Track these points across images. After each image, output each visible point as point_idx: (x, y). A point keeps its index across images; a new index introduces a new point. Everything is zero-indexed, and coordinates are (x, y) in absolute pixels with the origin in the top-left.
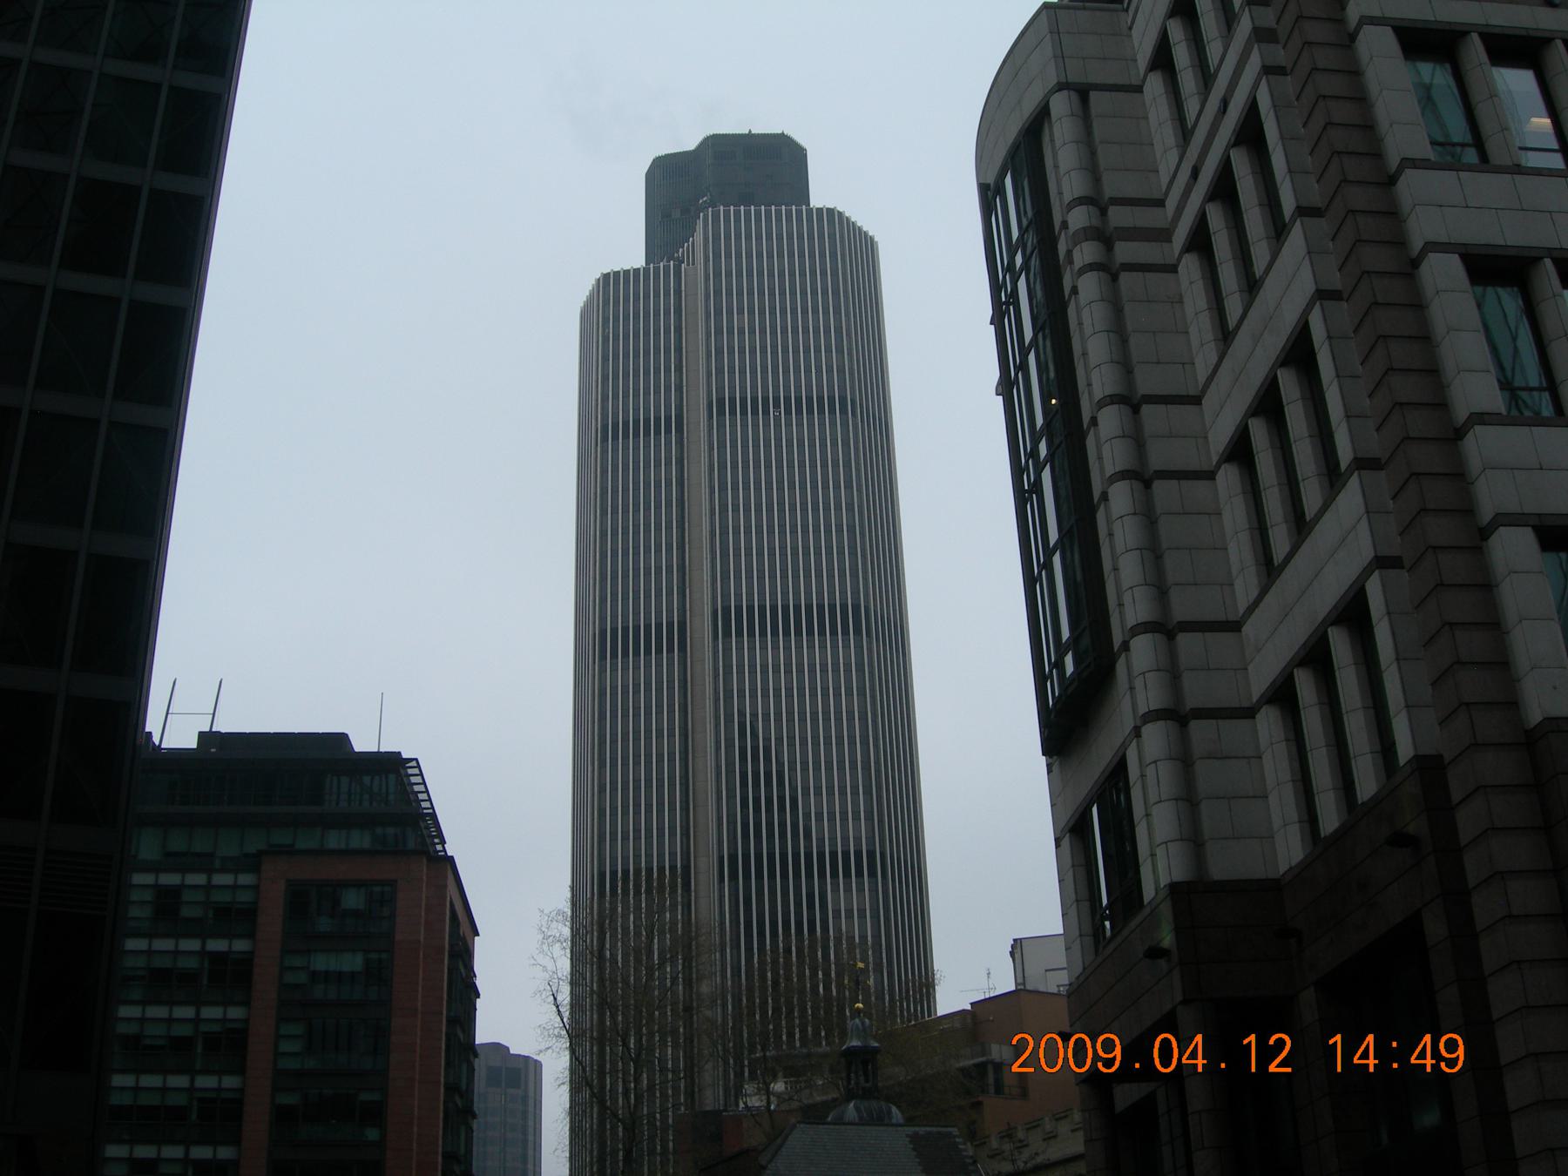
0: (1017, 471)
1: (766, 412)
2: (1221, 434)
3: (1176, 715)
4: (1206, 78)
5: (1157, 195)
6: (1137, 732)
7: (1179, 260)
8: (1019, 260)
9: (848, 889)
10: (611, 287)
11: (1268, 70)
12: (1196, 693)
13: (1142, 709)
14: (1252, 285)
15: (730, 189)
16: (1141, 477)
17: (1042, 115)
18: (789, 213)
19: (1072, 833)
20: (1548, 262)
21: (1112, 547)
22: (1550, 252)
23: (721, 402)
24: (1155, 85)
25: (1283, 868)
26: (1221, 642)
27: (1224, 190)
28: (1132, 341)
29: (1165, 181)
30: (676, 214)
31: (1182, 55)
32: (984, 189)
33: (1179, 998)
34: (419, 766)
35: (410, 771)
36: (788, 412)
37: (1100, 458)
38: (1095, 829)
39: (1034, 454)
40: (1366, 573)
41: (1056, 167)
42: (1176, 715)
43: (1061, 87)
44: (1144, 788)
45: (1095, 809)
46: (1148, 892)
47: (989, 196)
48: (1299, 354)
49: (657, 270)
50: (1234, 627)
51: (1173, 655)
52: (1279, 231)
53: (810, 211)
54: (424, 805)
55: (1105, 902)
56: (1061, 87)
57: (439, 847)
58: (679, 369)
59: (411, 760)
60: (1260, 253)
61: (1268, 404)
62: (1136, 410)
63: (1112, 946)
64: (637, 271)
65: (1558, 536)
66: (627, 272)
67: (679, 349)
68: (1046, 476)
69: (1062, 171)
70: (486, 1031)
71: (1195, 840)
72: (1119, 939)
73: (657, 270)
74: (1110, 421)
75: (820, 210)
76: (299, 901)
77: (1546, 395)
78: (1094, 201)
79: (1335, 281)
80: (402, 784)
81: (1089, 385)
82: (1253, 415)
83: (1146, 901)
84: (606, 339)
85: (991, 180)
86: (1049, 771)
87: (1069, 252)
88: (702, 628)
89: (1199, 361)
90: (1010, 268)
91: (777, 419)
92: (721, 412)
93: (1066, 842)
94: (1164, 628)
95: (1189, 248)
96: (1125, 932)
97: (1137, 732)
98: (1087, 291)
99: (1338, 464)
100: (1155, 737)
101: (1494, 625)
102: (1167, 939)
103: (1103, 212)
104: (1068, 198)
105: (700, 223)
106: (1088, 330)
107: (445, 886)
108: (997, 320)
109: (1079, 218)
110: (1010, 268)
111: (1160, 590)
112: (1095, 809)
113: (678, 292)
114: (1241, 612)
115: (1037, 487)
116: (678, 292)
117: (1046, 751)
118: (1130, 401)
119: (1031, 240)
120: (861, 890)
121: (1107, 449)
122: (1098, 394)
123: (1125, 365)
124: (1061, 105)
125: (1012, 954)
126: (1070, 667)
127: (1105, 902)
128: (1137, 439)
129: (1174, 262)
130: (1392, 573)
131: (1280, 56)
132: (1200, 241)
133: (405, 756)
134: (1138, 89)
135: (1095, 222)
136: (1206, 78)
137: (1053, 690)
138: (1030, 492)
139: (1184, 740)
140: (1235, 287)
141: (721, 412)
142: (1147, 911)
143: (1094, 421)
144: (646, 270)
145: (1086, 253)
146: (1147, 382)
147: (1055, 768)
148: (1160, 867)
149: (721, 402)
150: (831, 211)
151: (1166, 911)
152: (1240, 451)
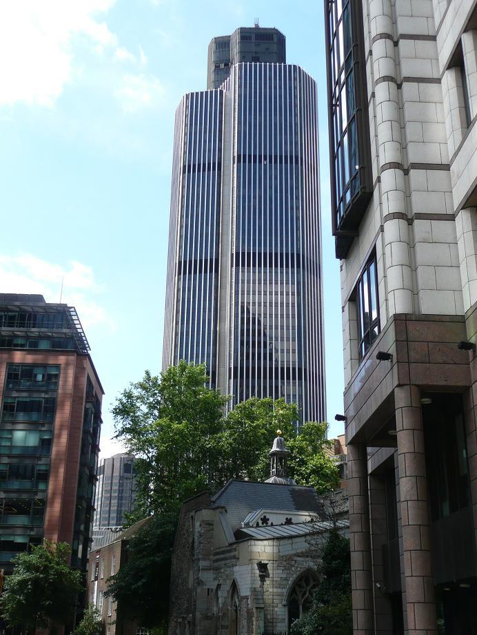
1: (260, 162)
3: (407, 218)
5: (431, 33)
8: (343, 77)
10: (194, 100)
12: (420, 204)
13: (385, 213)
16: (396, 81)
21: (384, 264)
25: (467, 307)
30: (222, 66)
33: (396, 383)
36: (270, 162)
44: (387, 306)
50: (446, 167)
51: (407, 184)
59: (72, 308)
62: (406, 172)
66: (202, 93)
71: (413, 292)
72: (368, 355)
75: (290, 66)
84: (178, 290)
89: (450, 142)
91: (265, 165)
94: (402, 167)
96: (371, 351)
98: (380, 94)
100: (393, 229)
102: (392, 350)
106: (379, 119)
110: (338, 83)
111: (403, 146)
117: (338, 256)
118: (393, 38)
121: (377, 65)
134: (438, 81)
139: (411, 233)
146: (404, 27)
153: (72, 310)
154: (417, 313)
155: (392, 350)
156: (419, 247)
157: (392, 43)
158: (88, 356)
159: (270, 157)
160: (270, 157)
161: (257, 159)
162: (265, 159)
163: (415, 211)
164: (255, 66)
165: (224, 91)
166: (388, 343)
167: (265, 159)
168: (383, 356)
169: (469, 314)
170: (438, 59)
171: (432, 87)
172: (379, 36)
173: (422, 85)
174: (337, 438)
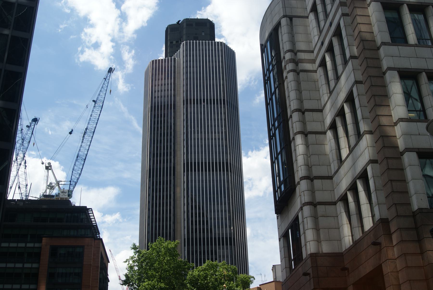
0: (269, 130)
2: (328, 121)
3: (313, 204)
4: (326, 16)
6: (301, 209)
7: (317, 69)
9: (223, 249)
11: (343, 15)
12: (320, 197)
13: (303, 202)
14: (338, 78)
15: (192, 34)
17: (278, 25)
18: (209, 43)
19: (284, 237)
20: (424, 73)
22: (424, 70)
23: (187, 100)
24: (312, 16)
26: (327, 182)
27: (330, 49)
28: (303, 93)
29: (314, 45)
30: (174, 42)
31: (320, 8)
32: (261, 45)
34: (92, 211)
35: (89, 212)
37: (292, 127)
38: (291, 236)
39: (274, 125)
40: (367, 164)
41: (282, 40)
42: (313, 204)
43: (284, 16)
45: (290, 230)
46: (304, 256)
47: (263, 48)
48: (350, 99)
49: (168, 59)
51: (313, 186)
52: (345, 63)
53: (215, 43)
54: (93, 222)
55: (292, 258)
56: (284, 16)
57: (98, 235)
58: (174, 90)
59: (90, 209)
60: (340, 68)
61: (341, 113)
63: (294, 272)
64: (162, 60)
65: (425, 155)
67: (174, 84)
68: (277, 132)
69: (284, 41)
70: (422, 15)
72: (296, 269)
73: (168, 59)
74: (296, 117)
75: (218, 43)
76: (54, 251)
77: (422, 113)
78: (294, 51)
79: (360, 78)
80: (87, 216)
81: (290, 106)
82: (337, 116)
83: (304, 258)
85: (263, 43)
86: (277, 219)
87: (285, 66)
88: (180, 168)
90: (268, 69)
91: (204, 106)
92: (187, 103)
93: (282, 240)
95: (320, 66)
96: (298, 267)
97: (301, 209)
99: (360, 132)
100: (307, 210)
101: (404, 181)
103: (296, 54)
104: (285, 50)
105: (182, 45)
106: (290, 89)
107: (100, 247)
108: (265, 83)
109: (288, 56)
112: (290, 230)
113: (175, 66)
114: (333, 173)
115: (274, 135)
116: (175, 66)
119: (274, 63)
120: (227, 249)
121: (295, 124)
122: (293, 108)
123: (300, 100)
124: (284, 22)
125: (272, 270)
126: (283, 189)
127: (292, 258)
128: (303, 122)
129: (316, 69)
130: (375, 165)
131: (347, 10)
132: (323, 64)
133: (88, 207)
134: (307, 17)
135: (293, 57)
136: (326, 16)
137: (278, 194)
138: (273, 136)
139: (316, 212)
140: (333, 78)
141: (187, 103)
142: (304, 261)
143: (291, 116)
144: (165, 60)
145: (290, 66)
146: (307, 105)
147: (279, 218)
148: (309, 247)
149: (187, 100)
150: (221, 43)
151: (309, 261)
152: (333, 127)
153: (90, 210)
154: (321, 252)
155: (310, 271)
156: (320, 219)
157: (302, 113)
158: (101, 240)
159: (207, 100)
160: (207, 100)
161: (199, 102)
162: (204, 102)
163: (317, 201)
164: (196, 43)
165: (177, 58)
166: (308, 266)
167: (204, 102)
168: (305, 274)
169: (345, 252)
170: (324, 122)
171: (322, 136)
172: (295, 110)
173: (318, 136)
174: (259, 286)
